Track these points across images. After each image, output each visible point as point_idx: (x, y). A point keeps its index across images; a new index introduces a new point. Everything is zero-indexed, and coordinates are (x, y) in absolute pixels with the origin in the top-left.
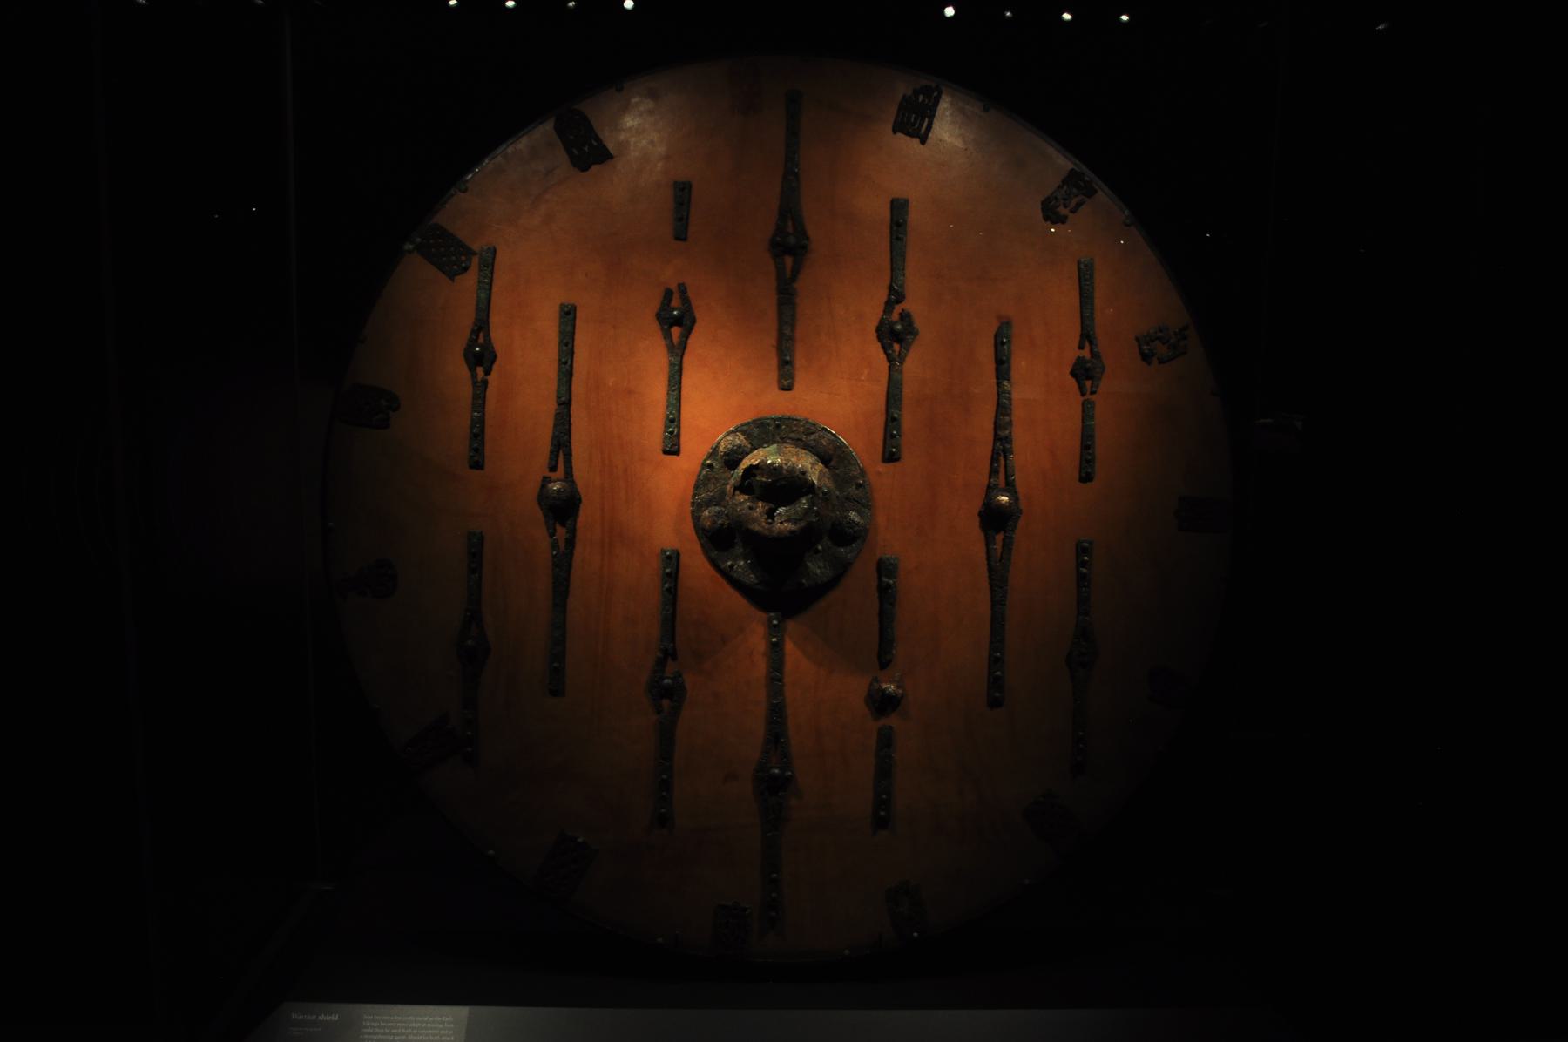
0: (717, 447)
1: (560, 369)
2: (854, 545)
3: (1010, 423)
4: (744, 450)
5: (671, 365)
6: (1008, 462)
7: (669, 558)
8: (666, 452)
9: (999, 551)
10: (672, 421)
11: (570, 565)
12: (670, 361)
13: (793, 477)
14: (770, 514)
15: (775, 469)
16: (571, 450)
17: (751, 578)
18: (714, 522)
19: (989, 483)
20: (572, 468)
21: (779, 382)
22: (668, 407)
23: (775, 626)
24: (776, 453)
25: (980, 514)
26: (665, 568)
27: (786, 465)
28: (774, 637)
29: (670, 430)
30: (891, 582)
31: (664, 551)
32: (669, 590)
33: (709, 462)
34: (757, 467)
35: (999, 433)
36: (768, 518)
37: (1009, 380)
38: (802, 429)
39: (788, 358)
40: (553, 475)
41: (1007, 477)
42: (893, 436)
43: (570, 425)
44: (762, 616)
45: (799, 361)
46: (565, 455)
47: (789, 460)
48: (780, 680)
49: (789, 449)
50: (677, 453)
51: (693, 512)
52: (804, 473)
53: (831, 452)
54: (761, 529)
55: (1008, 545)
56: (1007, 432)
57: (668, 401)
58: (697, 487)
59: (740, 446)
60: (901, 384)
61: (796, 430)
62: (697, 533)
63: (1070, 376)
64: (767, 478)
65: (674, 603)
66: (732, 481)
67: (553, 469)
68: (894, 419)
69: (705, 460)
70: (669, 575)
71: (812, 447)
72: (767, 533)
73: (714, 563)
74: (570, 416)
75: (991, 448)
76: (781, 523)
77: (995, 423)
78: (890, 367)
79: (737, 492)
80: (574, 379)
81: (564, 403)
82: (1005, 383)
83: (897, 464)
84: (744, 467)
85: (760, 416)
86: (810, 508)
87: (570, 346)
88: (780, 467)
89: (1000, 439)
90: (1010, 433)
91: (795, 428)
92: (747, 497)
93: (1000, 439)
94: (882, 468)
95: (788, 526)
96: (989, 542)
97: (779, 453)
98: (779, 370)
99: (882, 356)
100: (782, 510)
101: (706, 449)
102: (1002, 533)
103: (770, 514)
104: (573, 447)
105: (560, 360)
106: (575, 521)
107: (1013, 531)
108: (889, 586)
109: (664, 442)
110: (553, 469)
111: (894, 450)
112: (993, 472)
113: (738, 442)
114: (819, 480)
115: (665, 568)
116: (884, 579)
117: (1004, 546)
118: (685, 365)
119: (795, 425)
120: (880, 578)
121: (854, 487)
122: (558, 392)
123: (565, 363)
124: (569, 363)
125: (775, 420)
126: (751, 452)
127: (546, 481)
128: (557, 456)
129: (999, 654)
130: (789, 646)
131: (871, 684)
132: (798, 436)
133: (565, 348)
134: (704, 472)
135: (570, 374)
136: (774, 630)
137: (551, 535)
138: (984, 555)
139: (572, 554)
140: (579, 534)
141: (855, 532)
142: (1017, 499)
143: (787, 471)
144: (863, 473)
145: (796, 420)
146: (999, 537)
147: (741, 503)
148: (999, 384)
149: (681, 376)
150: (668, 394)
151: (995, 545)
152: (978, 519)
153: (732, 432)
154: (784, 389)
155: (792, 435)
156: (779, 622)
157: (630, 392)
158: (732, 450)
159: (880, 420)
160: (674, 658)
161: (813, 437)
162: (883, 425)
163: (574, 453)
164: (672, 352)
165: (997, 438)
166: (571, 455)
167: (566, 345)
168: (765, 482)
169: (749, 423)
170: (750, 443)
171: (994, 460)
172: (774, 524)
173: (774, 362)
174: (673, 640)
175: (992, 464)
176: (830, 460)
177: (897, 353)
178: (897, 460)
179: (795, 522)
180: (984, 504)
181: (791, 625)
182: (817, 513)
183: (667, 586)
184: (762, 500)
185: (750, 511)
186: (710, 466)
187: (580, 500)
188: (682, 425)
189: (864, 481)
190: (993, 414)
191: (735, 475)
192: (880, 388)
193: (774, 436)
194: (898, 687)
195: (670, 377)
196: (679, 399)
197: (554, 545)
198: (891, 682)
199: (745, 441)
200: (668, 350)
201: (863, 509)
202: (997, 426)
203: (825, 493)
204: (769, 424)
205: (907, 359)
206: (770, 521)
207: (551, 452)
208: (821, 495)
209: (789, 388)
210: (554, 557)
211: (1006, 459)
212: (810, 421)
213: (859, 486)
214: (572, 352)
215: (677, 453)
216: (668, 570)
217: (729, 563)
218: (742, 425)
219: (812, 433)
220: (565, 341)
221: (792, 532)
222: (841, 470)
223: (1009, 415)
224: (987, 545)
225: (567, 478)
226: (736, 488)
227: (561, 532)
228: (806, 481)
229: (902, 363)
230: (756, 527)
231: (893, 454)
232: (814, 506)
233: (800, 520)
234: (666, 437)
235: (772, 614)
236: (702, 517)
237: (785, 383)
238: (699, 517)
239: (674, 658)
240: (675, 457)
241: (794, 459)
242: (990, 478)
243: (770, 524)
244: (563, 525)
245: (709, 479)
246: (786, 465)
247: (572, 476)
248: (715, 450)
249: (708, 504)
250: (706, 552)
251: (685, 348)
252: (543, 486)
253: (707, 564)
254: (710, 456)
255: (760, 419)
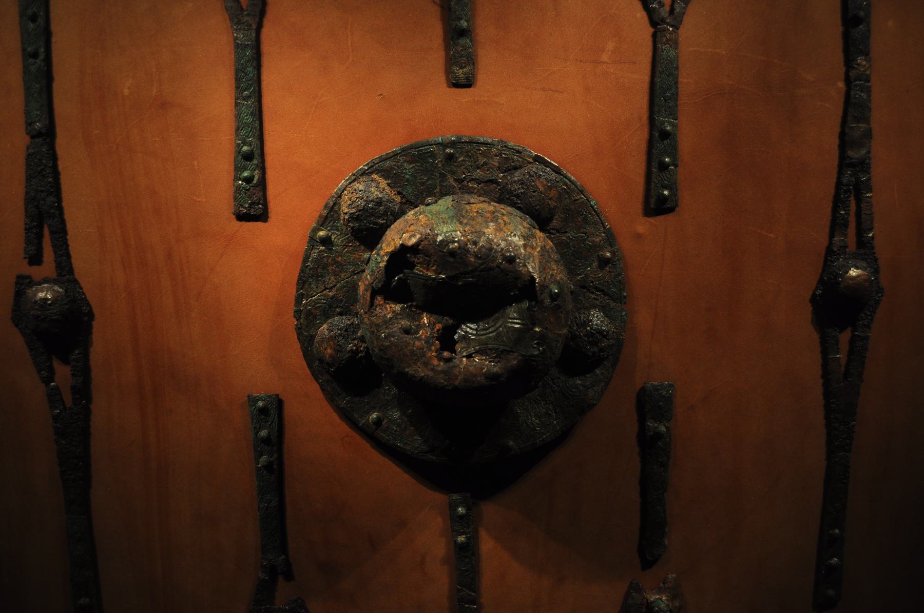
0: (335, 204)
1: (26, 70)
2: (598, 371)
3: (868, 134)
4: (388, 209)
5: (239, 47)
6: (863, 205)
7: (264, 411)
8: (241, 217)
9: (843, 362)
10: (248, 157)
11: (86, 432)
12: (236, 39)
13: (491, 269)
14: (447, 341)
15: (452, 253)
16: (63, 222)
17: (414, 443)
18: (339, 349)
19: (831, 243)
20: (69, 256)
21: (448, 71)
22: (237, 129)
23: (461, 517)
24: (452, 218)
25: (814, 300)
26: (257, 430)
27: (475, 243)
28: (461, 534)
29: (246, 174)
30: (663, 429)
31: (252, 400)
32: (268, 467)
33: (322, 233)
34: (415, 249)
35: (850, 153)
36: (443, 348)
37: (866, 54)
38: (495, 162)
39: (464, 24)
40: (35, 272)
41: (860, 232)
42: (663, 167)
43: (56, 174)
44: (440, 498)
45: (485, 30)
46: (52, 233)
47: (480, 234)
48: (473, 602)
49: (479, 205)
50: (263, 217)
51: (299, 329)
52: (511, 260)
53: (552, 204)
54: (430, 373)
55: (857, 350)
56: (863, 151)
57: (238, 116)
58: (302, 282)
59: (379, 202)
60: (677, 68)
61: (485, 164)
62: (310, 366)
63: (239, 223)
64: (436, 272)
65: (279, 487)
66: (367, 277)
67: (35, 259)
68: (665, 135)
69: (315, 230)
70: (267, 441)
71: (517, 196)
72: (441, 380)
73: (347, 416)
74: (54, 158)
75: (834, 180)
76: (469, 357)
77: (842, 135)
78: (654, 36)
79: (379, 300)
80: (56, 86)
81: (39, 134)
82: (860, 60)
83: (670, 217)
84: (390, 249)
85: (413, 141)
86: (527, 329)
87: (41, 21)
88: (463, 248)
89: (852, 165)
90: (869, 152)
91: (482, 160)
92: (398, 307)
93: (852, 165)
94: (643, 225)
95: (483, 364)
96: (827, 347)
97: (459, 216)
98: (447, 49)
99: (641, 15)
100: (470, 328)
101: (315, 208)
102: (849, 330)
103: (447, 341)
104: (67, 216)
105: (24, 50)
106: (86, 356)
107: (868, 326)
108: (658, 436)
109: (235, 199)
110: (35, 259)
111: (666, 193)
112: (837, 225)
113: (375, 193)
114: (543, 269)
115: (257, 430)
116: (650, 424)
117: (851, 352)
118: (265, 48)
119: (484, 154)
120: (642, 420)
121: (595, 264)
122: (27, 113)
123: (35, 55)
124: (42, 56)
125: (444, 145)
126: (403, 213)
127: (24, 283)
128: (40, 236)
129: (837, 531)
130: (487, 545)
131: (628, 595)
132: (488, 175)
133: (31, 26)
134: (314, 254)
135: (47, 76)
136: (459, 523)
137: (47, 380)
138: (818, 371)
139: (87, 412)
140: (97, 374)
141: (601, 350)
142: (876, 271)
143: (476, 256)
144: (611, 239)
145: (485, 144)
146: (845, 337)
147: (387, 323)
148: (849, 62)
149: (259, 67)
150: (237, 104)
151: (838, 353)
152: (809, 308)
153: (364, 173)
154: (457, 85)
155: (478, 174)
156: (469, 509)
157: (164, 105)
158: (364, 210)
159: (638, 138)
160: (289, 576)
161: (517, 176)
162: (644, 146)
163: (69, 226)
164: (239, 23)
165: (844, 163)
166: (64, 231)
167: (34, 18)
168: (434, 279)
169: (395, 154)
170: (399, 193)
171: (838, 202)
172: (456, 361)
173: (436, 31)
174: (283, 548)
175: (835, 209)
176: (550, 219)
177: (667, 8)
178: (671, 210)
179: (499, 355)
180: (821, 281)
181: (490, 510)
182: (542, 338)
183: (264, 459)
184: (431, 312)
185: (407, 338)
186: (326, 241)
187: (91, 315)
188: (269, 164)
189: (613, 253)
190: (838, 121)
191: (372, 264)
192: (640, 76)
193: (443, 176)
194: (673, 598)
195: (237, 71)
196: (259, 114)
197: (54, 397)
198: (660, 591)
199: (388, 189)
200: (231, 19)
201: (613, 304)
202: (844, 142)
203: (554, 297)
204: (433, 155)
205: (686, 19)
206: (446, 354)
207: (28, 230)
208: (547, 301)
209: (468, 84)
210: (56, 418)
211: (859, 200)
212: (511, 144)
213: (604, 262)
214: (47, 34)
215: (263, 217)
216: (264, 433)
217: (374, 416)
218: (382, 159)
219: (516, 168)
220: (30, 12)
221: (492, 377)
222: (571, 234)
223: (867, 120)
224: (825, 353)
225: (60, 275)
226: (374, 293)
227: (63, 372)
228: (518, 276)
229: (676, 28)
230: (421, 372)
231: (664, 199)
232: (534, 325)
233: (508, 352)
234: (238, 188)
235: (455, 497)
236: (317, 339)
237: (460, 72)
238: (312, 338)
239: (289, 576)
240: (260, 224)
241: (490, 230)
242: (832, 235)
243: (448, 360)
244: (65, 361)
245: (325, 267)
246: (475, 243)
247: (71, 271)
248: (330, 215)
249: (327, 313)
250: (331, 398)
251: (262, 13)
252: (19, 294)
253: (335, 417)
254: (323, 222)
255: (412, 147)
